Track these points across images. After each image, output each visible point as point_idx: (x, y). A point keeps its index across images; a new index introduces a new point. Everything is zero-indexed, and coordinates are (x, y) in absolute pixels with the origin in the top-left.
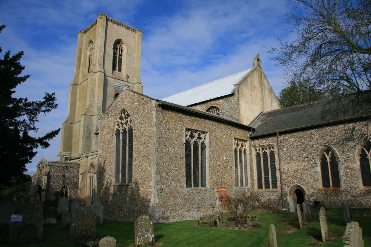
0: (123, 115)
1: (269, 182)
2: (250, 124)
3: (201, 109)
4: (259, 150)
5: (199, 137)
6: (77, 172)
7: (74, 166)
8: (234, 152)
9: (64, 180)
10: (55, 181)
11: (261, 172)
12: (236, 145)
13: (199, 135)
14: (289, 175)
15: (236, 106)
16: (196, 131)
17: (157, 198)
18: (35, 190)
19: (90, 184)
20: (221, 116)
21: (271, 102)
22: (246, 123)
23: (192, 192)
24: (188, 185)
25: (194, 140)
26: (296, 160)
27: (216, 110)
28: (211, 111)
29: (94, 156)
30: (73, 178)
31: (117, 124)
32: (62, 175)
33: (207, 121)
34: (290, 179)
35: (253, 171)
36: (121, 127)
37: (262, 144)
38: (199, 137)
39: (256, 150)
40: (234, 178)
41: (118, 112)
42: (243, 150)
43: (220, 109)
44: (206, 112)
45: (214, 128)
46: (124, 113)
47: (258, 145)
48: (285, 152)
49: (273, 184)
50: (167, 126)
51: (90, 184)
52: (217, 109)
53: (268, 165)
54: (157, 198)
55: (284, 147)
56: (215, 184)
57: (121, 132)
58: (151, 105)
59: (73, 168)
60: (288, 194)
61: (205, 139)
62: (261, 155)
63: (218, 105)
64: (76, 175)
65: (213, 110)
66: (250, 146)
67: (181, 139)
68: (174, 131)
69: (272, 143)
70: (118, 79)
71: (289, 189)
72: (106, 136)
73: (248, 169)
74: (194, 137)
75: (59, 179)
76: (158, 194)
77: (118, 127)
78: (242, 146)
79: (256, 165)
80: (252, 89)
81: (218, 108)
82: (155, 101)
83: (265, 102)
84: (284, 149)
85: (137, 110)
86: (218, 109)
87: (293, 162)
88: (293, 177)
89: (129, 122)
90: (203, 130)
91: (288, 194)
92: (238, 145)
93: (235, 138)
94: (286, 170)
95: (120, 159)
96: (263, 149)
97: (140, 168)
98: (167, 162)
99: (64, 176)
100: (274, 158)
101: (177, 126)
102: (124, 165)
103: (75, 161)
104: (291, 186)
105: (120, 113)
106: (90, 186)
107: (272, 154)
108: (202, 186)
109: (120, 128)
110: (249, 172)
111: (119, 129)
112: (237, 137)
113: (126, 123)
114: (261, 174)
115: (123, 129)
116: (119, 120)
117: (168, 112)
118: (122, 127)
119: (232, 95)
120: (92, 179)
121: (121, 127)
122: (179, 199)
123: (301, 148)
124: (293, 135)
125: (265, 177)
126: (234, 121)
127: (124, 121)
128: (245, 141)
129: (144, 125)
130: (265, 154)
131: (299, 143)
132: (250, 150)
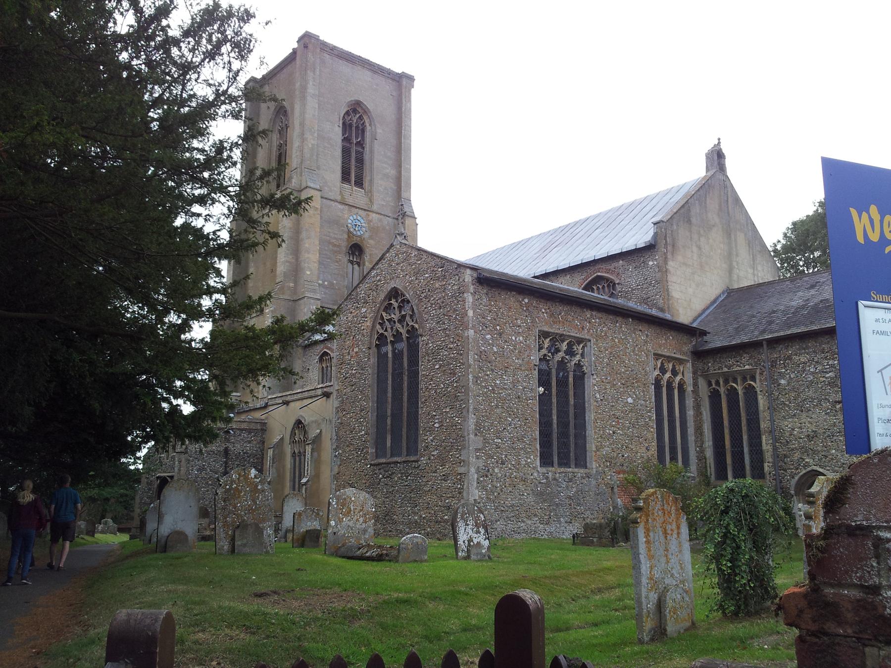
0: (393, 301)
1: (744, 462)
2: (694, 320)
3: (572, 286)
4: (718, 383)
5: (570, 352)
6: (258, 443)
7: (252, 426)
8: (653, 387)
9: (226, 463)
10: (204, 465)
11: (724, 438)
12: (657, 372)
13: (570, 345)
14: (795, 444)
15: (658, 275)
16: (562, 338)
17: (477, 488)
18: (150, 489)
19: (294, 473)
20: (620, 301)
21: (752, 262)
22: (684, 317)
23: (555, 479)
24: (546, 460)
25: (559, 356)
26: (814, 408)
27: (609, 286)
28: (595, 287)
29: (305, 401)
30: (248, 457)
31: (379, 323)
32: (222, 449)
33: (588, 314)
34: (797, 455)
35: (701, 434)
36: (389, 330)
37: (726, 370)
38: (570, 352)
39: (710, 384)
40: (654, 450)
41: (382, 296)
42: (677, 383)
43: (618, 284)
44: (584, 291)
45: (604, 329)
46: (396, 298)
47: (715, 370)
48: (786, 389)
49: (753, 467)
50: (498, 328)
51: (294, 473)
52: (611, 282)
53: (740, 420)
54: (477, 488)
55: (782, 376)
56: (606, 461)
57: (389, 341)
58: (461, 280)
59: (250, 433)
60: (793, 492)
61: (582, 355)
62: (722, 396)
63: (612, 273)
64: (257, 451)
65: (600, 287)
66: (694, 373)
67: (528, 356)
68: (514, 338)
69: (751, 367)
70: (356, 208)
71: (794, 482)
72: (353, 350)
73: (691, 430)
74: (558, 351)
75: (214, 461)
76: (477, 479)
77: (383, 328)
78: (675, 373)
79: (709, 420)
80: (702, 232)
81: (612, 282)
82: (468, 271)
83: (735, 264)
84: (783, 382)
85: (429, 290)
86: (612, 284)
87: (804, 415)
88: (805, 450)
89: (408, 318)
90: (577, 335)
91: (793, 492)
92: (663, 370)
93: (654, 354)
94: (787, 434)
95: (386, 401)
96: (726, 382)
97: (437, 421)
98: (497, 406)
99: (226, 451)
100: (757, 403)
101: (519, 326)
102: (396, 416)
103: (258, 415)
104: (801, 474)
105: (388, 297)
106: (292, 476)
107: (751, 393)
108: (577, 466)
109: (386, 330)
110: (691, 438)
111: (386, 333)
112: (660, 352)
113: (402, 319)
114: (724, 442)
115: (393, 335)
116: (384, 314)
117: (499, 294)
118: (392, 328)
119: (650, 248)
120: (300, 460)
121: (389, 330)
122: (526, 494)
123: (826, 378)
124: (804, 346)
125: (733, 452)
126: (654, 312)
127: (395, 317)
128: (681, 361)
129: (445, 324)
130: (732, 393)
131: (820, 368)
132: (695, 385)
